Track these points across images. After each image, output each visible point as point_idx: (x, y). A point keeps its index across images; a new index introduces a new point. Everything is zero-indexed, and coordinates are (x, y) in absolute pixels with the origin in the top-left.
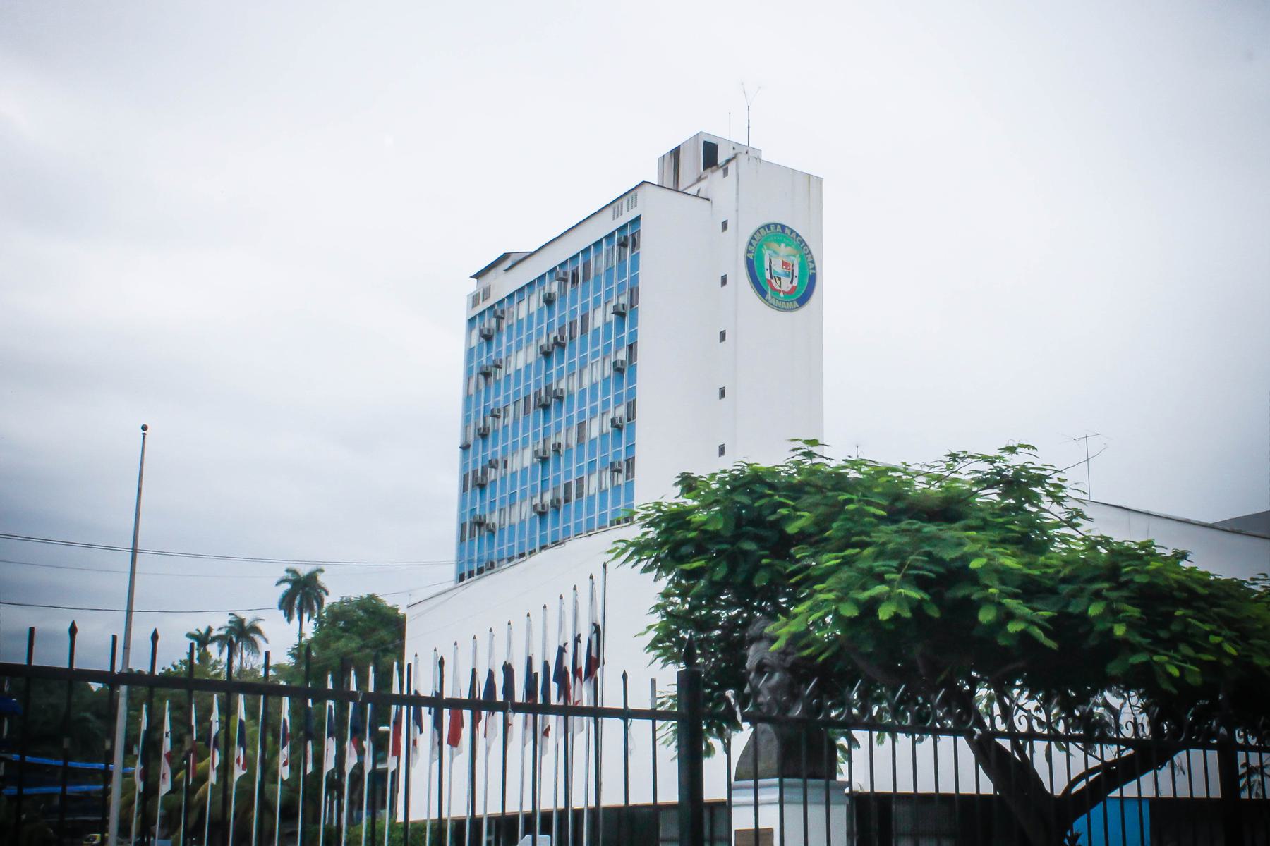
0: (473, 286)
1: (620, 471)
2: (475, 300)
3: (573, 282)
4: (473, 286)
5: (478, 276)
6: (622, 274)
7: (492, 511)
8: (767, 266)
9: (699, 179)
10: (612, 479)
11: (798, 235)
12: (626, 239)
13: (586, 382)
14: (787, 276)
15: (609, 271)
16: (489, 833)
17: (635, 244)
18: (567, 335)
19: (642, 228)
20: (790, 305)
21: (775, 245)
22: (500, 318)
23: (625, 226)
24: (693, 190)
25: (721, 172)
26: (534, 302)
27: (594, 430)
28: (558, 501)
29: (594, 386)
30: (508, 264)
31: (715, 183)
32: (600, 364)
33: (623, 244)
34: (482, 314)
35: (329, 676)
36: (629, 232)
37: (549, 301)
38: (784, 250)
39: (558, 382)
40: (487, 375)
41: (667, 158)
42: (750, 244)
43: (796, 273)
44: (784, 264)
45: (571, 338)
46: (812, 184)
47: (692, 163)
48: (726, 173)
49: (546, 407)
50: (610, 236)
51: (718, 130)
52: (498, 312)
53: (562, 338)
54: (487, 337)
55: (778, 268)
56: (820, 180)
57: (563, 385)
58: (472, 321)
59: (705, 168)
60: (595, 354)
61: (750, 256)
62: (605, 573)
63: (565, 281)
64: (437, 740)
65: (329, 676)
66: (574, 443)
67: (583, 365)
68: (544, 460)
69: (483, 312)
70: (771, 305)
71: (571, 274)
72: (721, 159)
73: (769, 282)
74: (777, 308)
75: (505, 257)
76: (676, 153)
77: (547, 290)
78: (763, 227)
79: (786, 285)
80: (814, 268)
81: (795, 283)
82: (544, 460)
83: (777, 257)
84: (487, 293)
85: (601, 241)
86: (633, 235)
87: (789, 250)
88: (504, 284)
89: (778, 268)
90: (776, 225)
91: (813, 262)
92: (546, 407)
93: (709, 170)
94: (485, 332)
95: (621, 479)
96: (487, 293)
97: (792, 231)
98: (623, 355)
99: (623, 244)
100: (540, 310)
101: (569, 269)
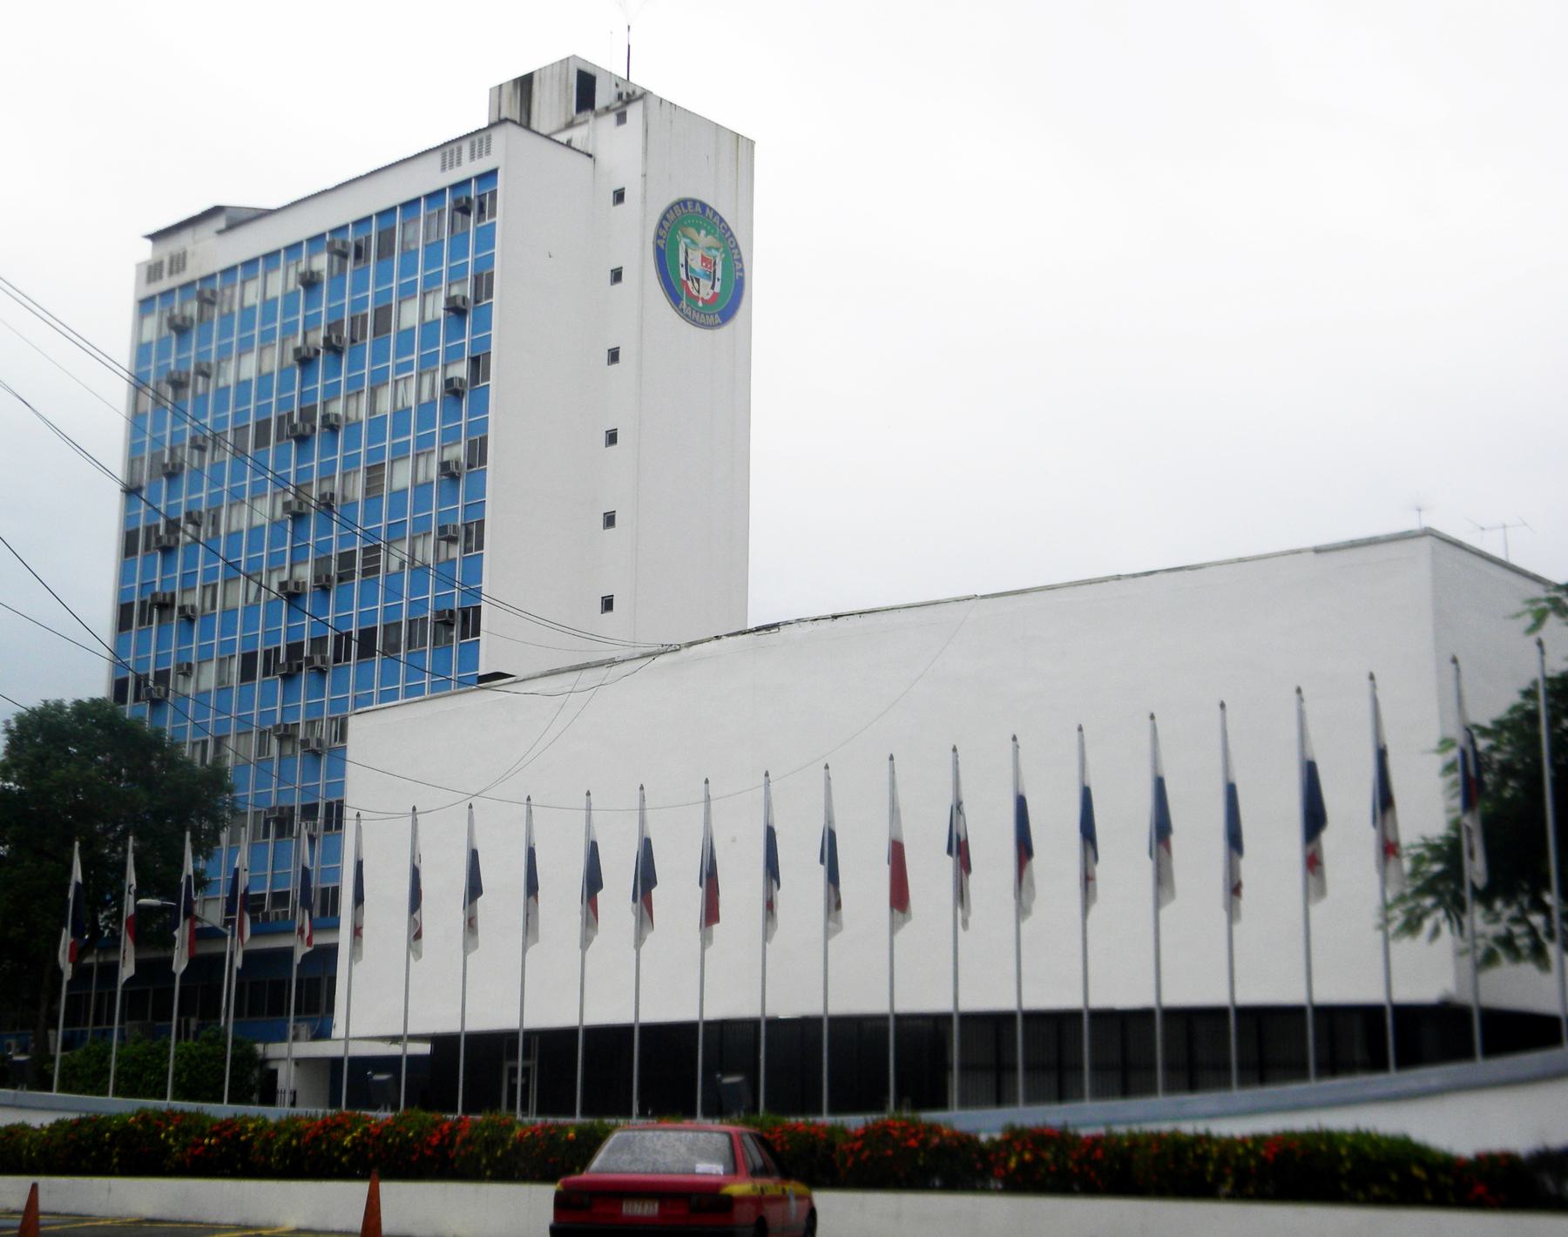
0: (146, 251)
1: (452, 540)
2: (153, 272)
3: (358, 255)
4: (146, 251)
5: (156, 237)
6: (459, 249)
7: (187, 588)
8: (682, 260)
9: (570, 125)
10: (437, 550)
11: (722, 220)
12: (471, 202)
13: (385, 405)
14: (708, 277)
15: (433, 250)
16: (526, 1056)
17: (485, 206)
18: (346, 334)
19: (500, 186)
20: (710, 320)
21: (692, 231)
22: (207, 301)
23: (467, 182)
24: (563, 137)
25: (612, 117)
26: (279, 283)
27: (401, 476)
28: (328, 578)
29: (401, 415)
30: (220, 223)
31: (599, 132)
32: (413, 384)
33: (463, 209)
34: (167, 294)
35: (188, 834)
36: (473, 192)
37: (310, 282)
38: (703, 238)
39: (325, 404)
40: (178, 384)
41: (506, 92)
42: (661, 226)
43: (719, 274)
44: (704, 259)
45: (353, 341)
46: (741, 147)
47: (551, 106)
48: (622, 118)
49: (303, 440)
50: (435, 196)
51: (606, 60)
52: (206, 291)
53: (339, 338)
54: (181, 329)
55: (696, 264)
56: (752, 143)
57: (337, 408)
58: (145, 305)
59: (579, 110)
60: (400, 368)
61: (662, 243)
62: (1542, 652)
63: (344, 256)
64: (833, 900)
65: (188, 834)
66: (359, 494)
67: (379, 381)
68: (299, 517)
69: (171, 292)
70: (686, 317)
71: (361, 244)
72: (603, 97)
73: (684, 283)
74: (695, 323)
75: (216, 211)
76: (525, 84)
77: (302, 267)
78: (678, 203)
79: (706, 290)
80: (742, 270)
81: (717, 289)
82: (299, 517)
83: (695, 251)
84: (178, 263)
85: (417, 201)
86: (481, 198)
87: (710, 241)
88: (212, 253)
89: (696, 264)
90: (694, 202)
91: (740, 260)
92: (303, 440)
93: (581, 117)
94: (178, 321)
95: (456, 552)
96: (178, 263)
97: (715, 213)
98: (461, 370)
99: (463, 209)
100: (290, 297)
101: (350, 237)
